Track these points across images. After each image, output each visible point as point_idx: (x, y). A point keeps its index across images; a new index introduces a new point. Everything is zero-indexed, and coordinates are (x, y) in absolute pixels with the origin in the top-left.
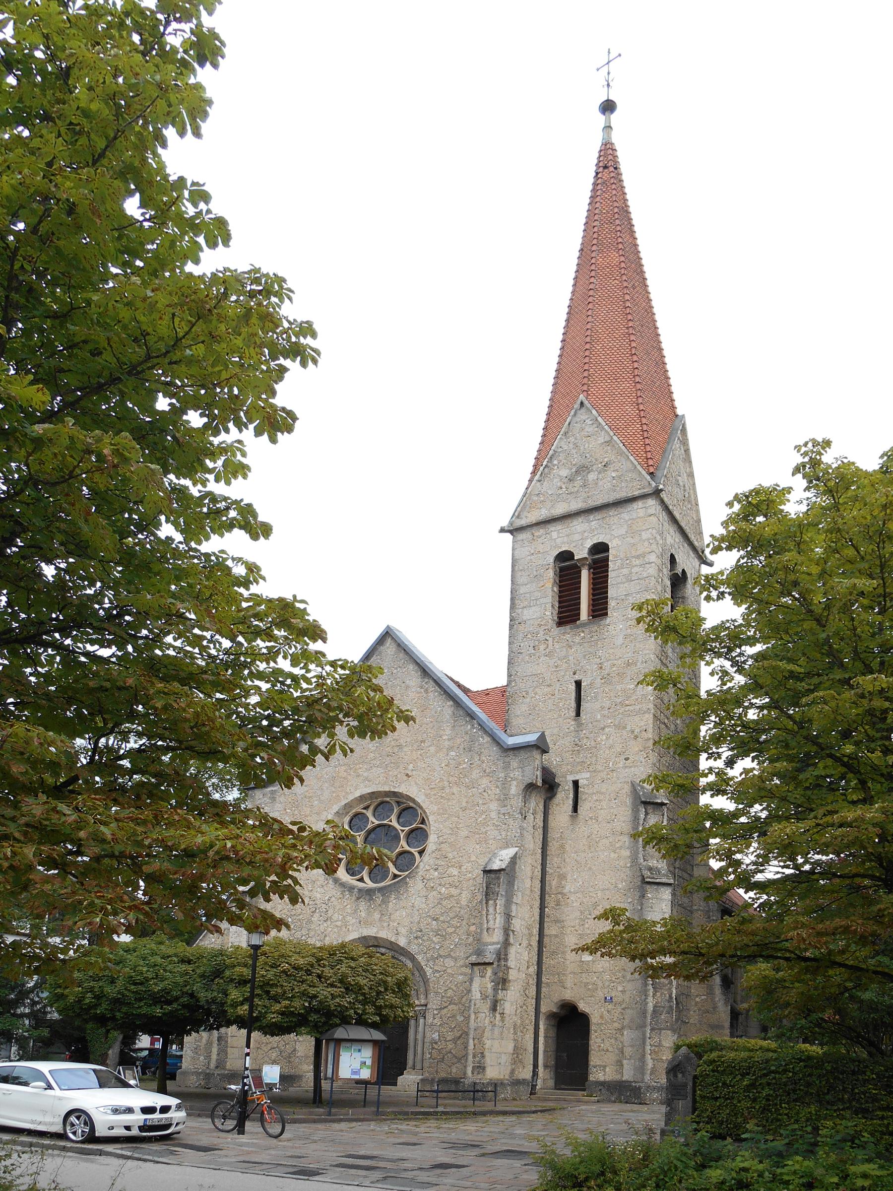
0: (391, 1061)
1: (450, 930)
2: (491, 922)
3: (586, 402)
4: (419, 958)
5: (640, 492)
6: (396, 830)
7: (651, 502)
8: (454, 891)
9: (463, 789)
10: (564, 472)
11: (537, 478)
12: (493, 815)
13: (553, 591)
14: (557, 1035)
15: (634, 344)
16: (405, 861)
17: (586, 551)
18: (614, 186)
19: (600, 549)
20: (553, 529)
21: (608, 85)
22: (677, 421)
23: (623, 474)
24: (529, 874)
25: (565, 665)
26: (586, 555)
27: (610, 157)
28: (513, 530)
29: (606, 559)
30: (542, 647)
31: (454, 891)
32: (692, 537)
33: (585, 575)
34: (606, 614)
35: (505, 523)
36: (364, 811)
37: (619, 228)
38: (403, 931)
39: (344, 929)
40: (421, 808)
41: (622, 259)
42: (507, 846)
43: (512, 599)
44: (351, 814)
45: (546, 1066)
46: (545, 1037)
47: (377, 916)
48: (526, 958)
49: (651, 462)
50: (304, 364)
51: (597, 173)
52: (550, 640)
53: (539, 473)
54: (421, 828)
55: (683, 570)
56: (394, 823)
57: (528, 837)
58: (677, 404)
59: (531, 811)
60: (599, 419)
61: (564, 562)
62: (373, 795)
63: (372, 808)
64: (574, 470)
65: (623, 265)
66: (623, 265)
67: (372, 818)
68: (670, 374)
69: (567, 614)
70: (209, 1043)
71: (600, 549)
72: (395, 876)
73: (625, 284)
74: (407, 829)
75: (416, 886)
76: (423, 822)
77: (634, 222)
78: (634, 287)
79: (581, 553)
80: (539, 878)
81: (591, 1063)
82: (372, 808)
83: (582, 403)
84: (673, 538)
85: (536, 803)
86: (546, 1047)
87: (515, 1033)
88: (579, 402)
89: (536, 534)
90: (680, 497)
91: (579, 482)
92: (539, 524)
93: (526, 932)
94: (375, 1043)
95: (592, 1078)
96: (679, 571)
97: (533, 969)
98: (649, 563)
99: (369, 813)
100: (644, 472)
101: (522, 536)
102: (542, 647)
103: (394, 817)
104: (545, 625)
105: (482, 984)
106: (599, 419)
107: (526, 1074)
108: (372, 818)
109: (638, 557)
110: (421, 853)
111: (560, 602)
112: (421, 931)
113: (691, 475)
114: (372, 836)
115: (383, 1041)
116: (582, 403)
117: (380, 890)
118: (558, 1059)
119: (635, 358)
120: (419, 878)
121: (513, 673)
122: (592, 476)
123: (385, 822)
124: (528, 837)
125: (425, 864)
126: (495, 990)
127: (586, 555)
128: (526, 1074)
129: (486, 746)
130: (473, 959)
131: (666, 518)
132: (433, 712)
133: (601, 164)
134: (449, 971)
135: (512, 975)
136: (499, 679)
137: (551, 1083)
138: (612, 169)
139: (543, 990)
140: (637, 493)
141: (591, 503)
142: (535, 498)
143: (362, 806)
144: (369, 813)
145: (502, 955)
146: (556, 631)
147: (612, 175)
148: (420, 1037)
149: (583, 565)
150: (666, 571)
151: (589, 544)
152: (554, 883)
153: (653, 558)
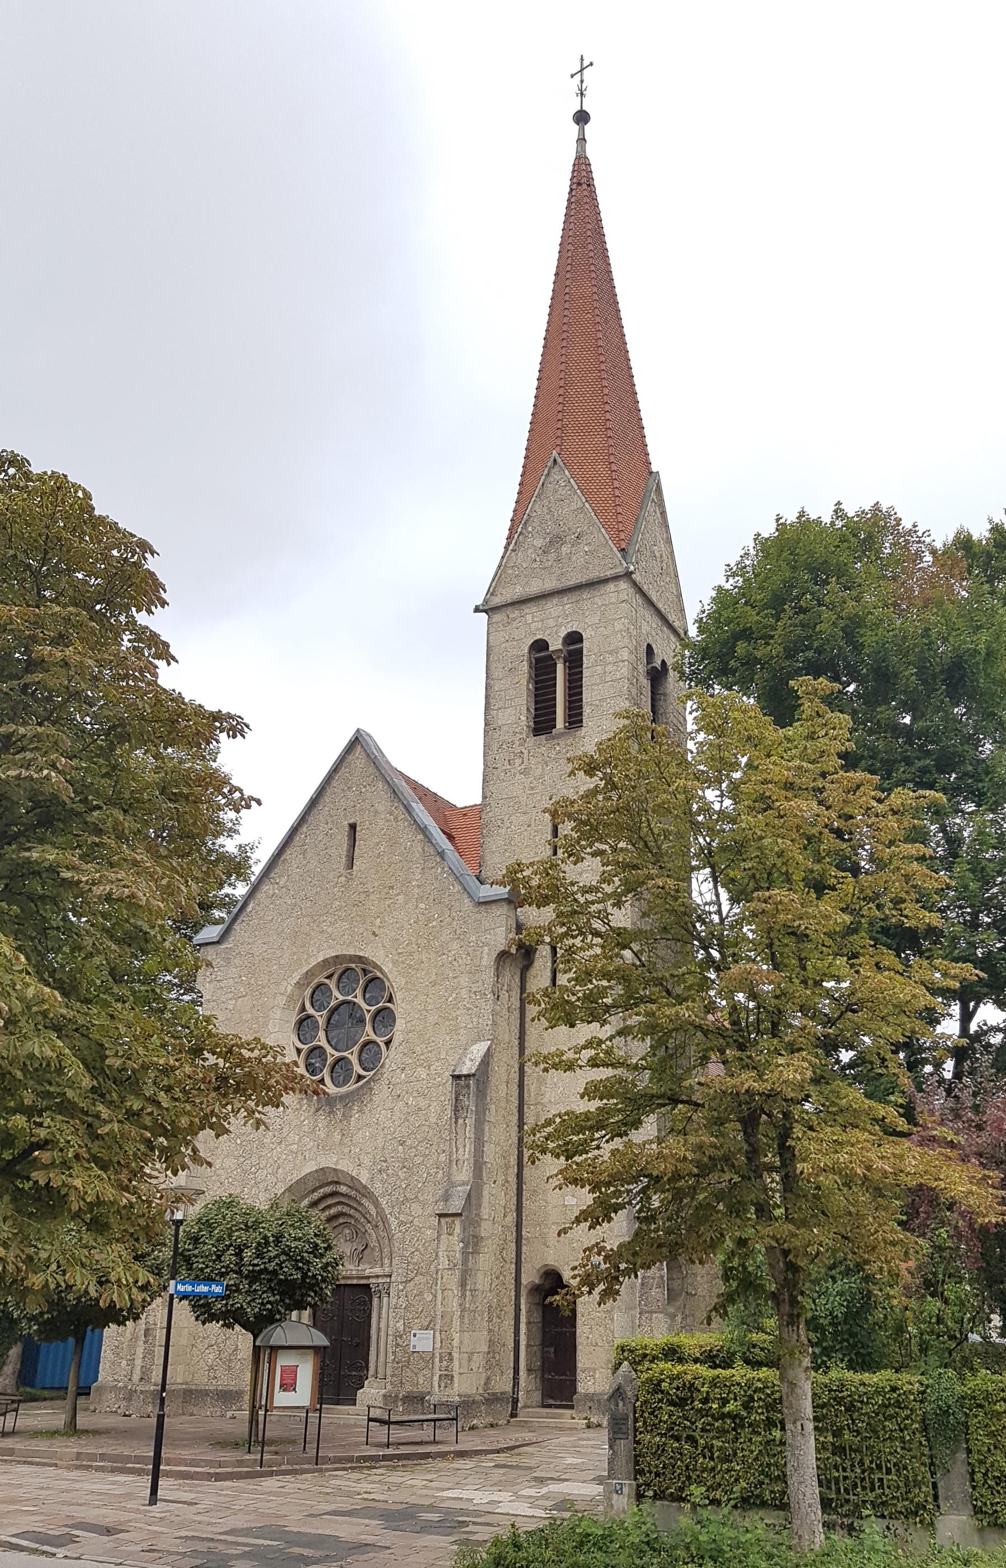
0: (341, 1373)
1: (418, 1160)
2: (461, 1150)
3: (559, 460)
4: (383, 1202)
5: (612, 572)
6: (362, 1010)
7: (623, 585)
8: (423, 1103)
9: (433, 956)
10: (539, 543)
11: (511, 548)
12: (464, 993)
13: (528, 689)
14: (544, 1317)
15: (606, 391)
16: (371, 1055)
17: (560, 641)
18: (587, 206)
19: (574, 638)
20: (527, 611)
21: (582, 94)
22: (651, 479)
23: (593, 553)
24: (504, 1078)
25: (541, 787)
26: (560, 647)
27: (584, 173)
28: (486, 608)
29: (580, 651)
30: (518, 761)
31: (423, 1103)
32: (671, 617)
33: (560, 668)
34: (581, 721)
35: (480, 601)
36: (327, 981)
37: (592, 254)
38: (366, 1161)
39: (300, 1157)
40: (388, 980)
41: (595, 289)
42: (478, 1040)
43: (487, 697)
44: (313, 985)
45: (529, 1370)
46: (528, 1323)
47: (338, 1137)
48: (503, 1203)
49: (622, 536)
50: (169, 664)
51: (571, 190)
52: (526, 752)
53: (514, 541)
54: (388, 1008)
55: (663, 661)
56: (359, 1000)
57: (502, 1023)
58: (652, 458)
59: (505, 988)
60: (572, 480)
61: (539, 651)
62: (337, 959)
63: (336, 977)
64: (548, 540)
65: (595, 297)
66: (595, 297)
67: (336, 993)
68: (644, 423)
69: (542, 723)
70: (134, 1338)
71: (574, 638)
72: (360, 1077)
73: (598, 319)
74: (373, 1008)
75: (381, 1093)
76: (390, 1000)
77: (608, 246)
78: (606, 321)
79: (556, 644)
80: (517, 1080)
81: (579, 1365)
82: (336, 977)
83: (555, 460)
84: (649, 626)
85: (511, 976)
86: (528, 1340)
87: (490, 1320)
88: (552, 459)
89: (511, 616)
90: (658, 570)
91: (552, 556)
92: (513, 604)
93: (501, 1162)
94: (316, 1349)
95: (581, 1388)
96: (657, 663)
97: (511, 1218)
98: (623, 661)
99: (332, 984)
100: (615, 549)
101: (498, 617)
102: (518, 761)
103: (359, 992)
104: (521, 733)
105: (453, 1243)
106: (572, 480)
107: (504, 1384)
108: (336, 993)
109: (611, 653)
110: (388, 1043)
111: (536, 703)
112: (385, 1161)
113: (669, 541)
114: (336, 1017)
115: (325, 1347)
116: (555, 460)
117: (342, 1098)
118: (544, 1359)
119: (607, 408)
120: (384, 1082)
121: (488, 794)
122: (565, 549)
123: (349, 998)
124: (502, 1023)
125: (392, 1059)
126: (465, 1253)
127: (560, 647)
128: (504, 1384)
129: (457, 896)
130: (441, 1208)
131: (640, 601)
132: (402, 848)
133: (575, 180)
134: (416, 1222)
135: (486, 1229)
136: (478, 800)
137: (537, 1396)
138: (585, 186)
139: (524, 1248)
140: (609, 573)
141: (560, 586)
142: (510, 572)
143: (326, 973)
144: (332, 984)
145: (473, 1198)
146: (532, 740)
147: (586, 193)
148: (383, 1325)
149: (559, 658)
150: (642, 669)
151: (563, 634)
152: (533, 1088)
153: (625, 654)
